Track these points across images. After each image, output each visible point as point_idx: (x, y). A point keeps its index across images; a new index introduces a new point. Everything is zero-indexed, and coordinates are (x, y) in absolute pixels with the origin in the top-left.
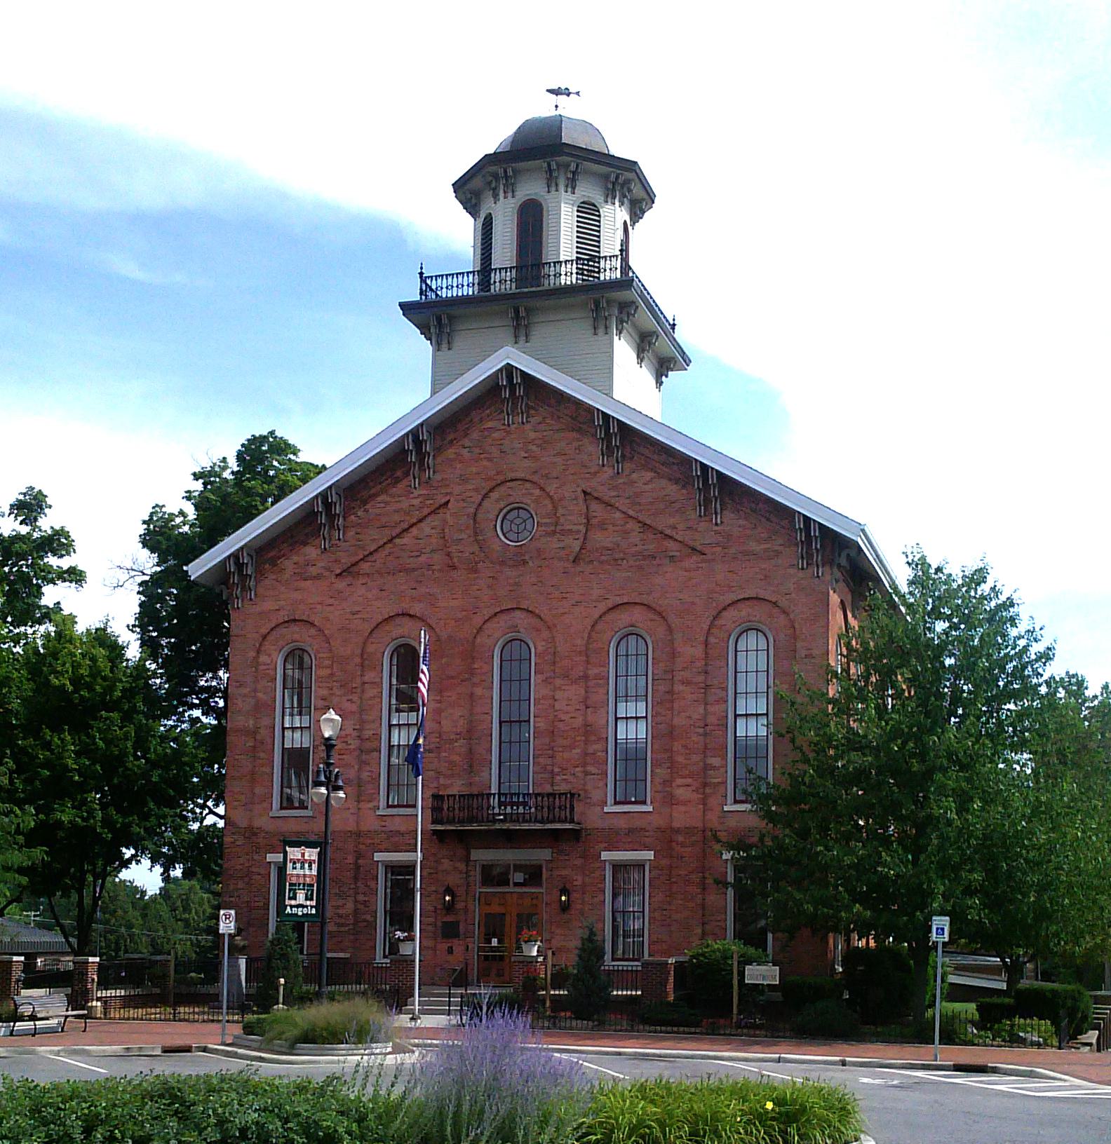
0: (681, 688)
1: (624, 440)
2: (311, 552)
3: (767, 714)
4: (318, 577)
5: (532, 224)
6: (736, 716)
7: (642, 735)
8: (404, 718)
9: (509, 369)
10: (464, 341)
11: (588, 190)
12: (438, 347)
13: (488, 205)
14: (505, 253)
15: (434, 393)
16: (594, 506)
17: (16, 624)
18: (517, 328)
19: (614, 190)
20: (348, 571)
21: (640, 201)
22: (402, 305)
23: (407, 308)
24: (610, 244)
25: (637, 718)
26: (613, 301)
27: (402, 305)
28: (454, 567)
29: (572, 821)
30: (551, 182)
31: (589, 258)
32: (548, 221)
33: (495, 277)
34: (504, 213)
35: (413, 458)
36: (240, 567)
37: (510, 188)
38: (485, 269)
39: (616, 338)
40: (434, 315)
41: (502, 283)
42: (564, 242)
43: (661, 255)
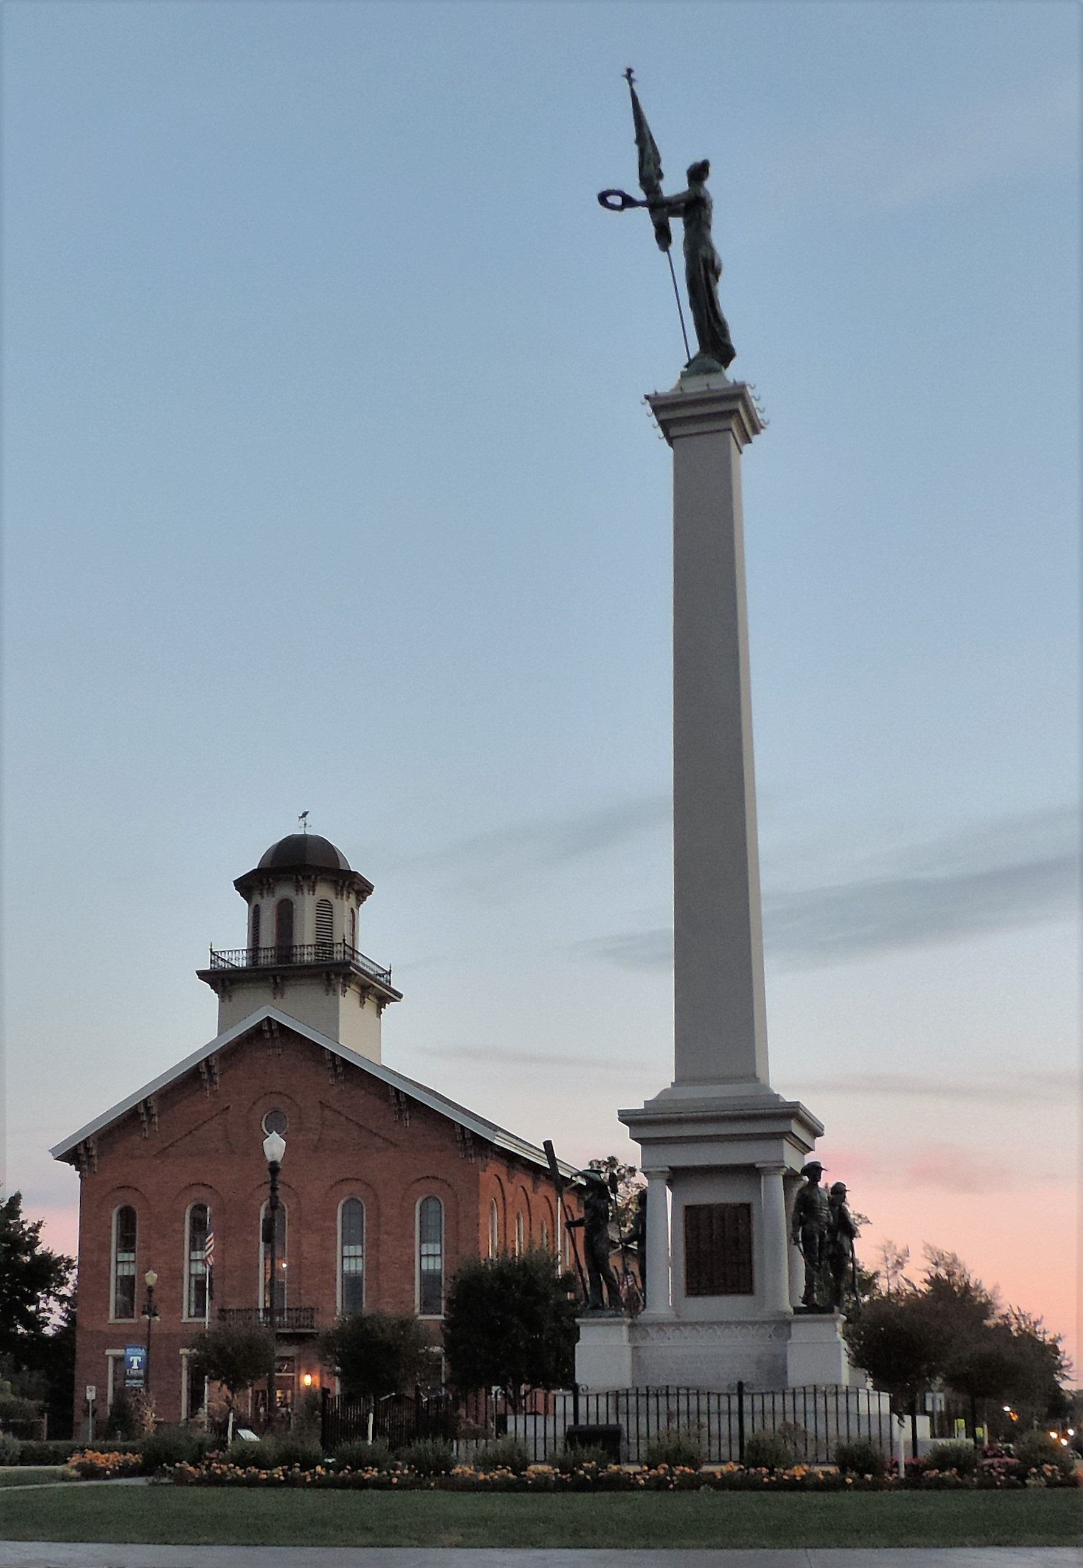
0: (386, 1236)
1: (348, 1072)
2: (136, 1139)
3: (440, 1255)
4: (141, 1157)
5: (286, 915)
6: (421, 1256)
7: (360, 1268)
8: (126, 1257)
9: (269, 1020)
10: (242, 996)
11: (324, 891)
12: (222, 998)
13: (257, 899)
14: (268, 939)
15: (219, 1034)
16: (327, 1112)
17: (1005, 1441)
18: (297, 891)
19: (342, 890)
20: (162, 1153)
21: (363, 891)
22: (198, 973)
23: (202, 975)
24: (341, 930)
25: (434, 1256)
26: (338, 970)
27: (198, 973)
28: (233, 1152)
29: (312, 1327)
30: (299, 888)
31: (324, 945)
32: (297, 915)
33: (262, 954)
34: (269, 906)
35: (206, 1077)
36: (87, 1149)
37: (271, 890)
38: (254, 949)
39: (341, 997)
40: (221, 979)
41: (266, 959)
42: (306, 934)
43: (377, 934)
